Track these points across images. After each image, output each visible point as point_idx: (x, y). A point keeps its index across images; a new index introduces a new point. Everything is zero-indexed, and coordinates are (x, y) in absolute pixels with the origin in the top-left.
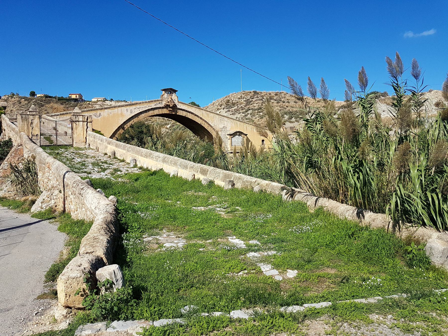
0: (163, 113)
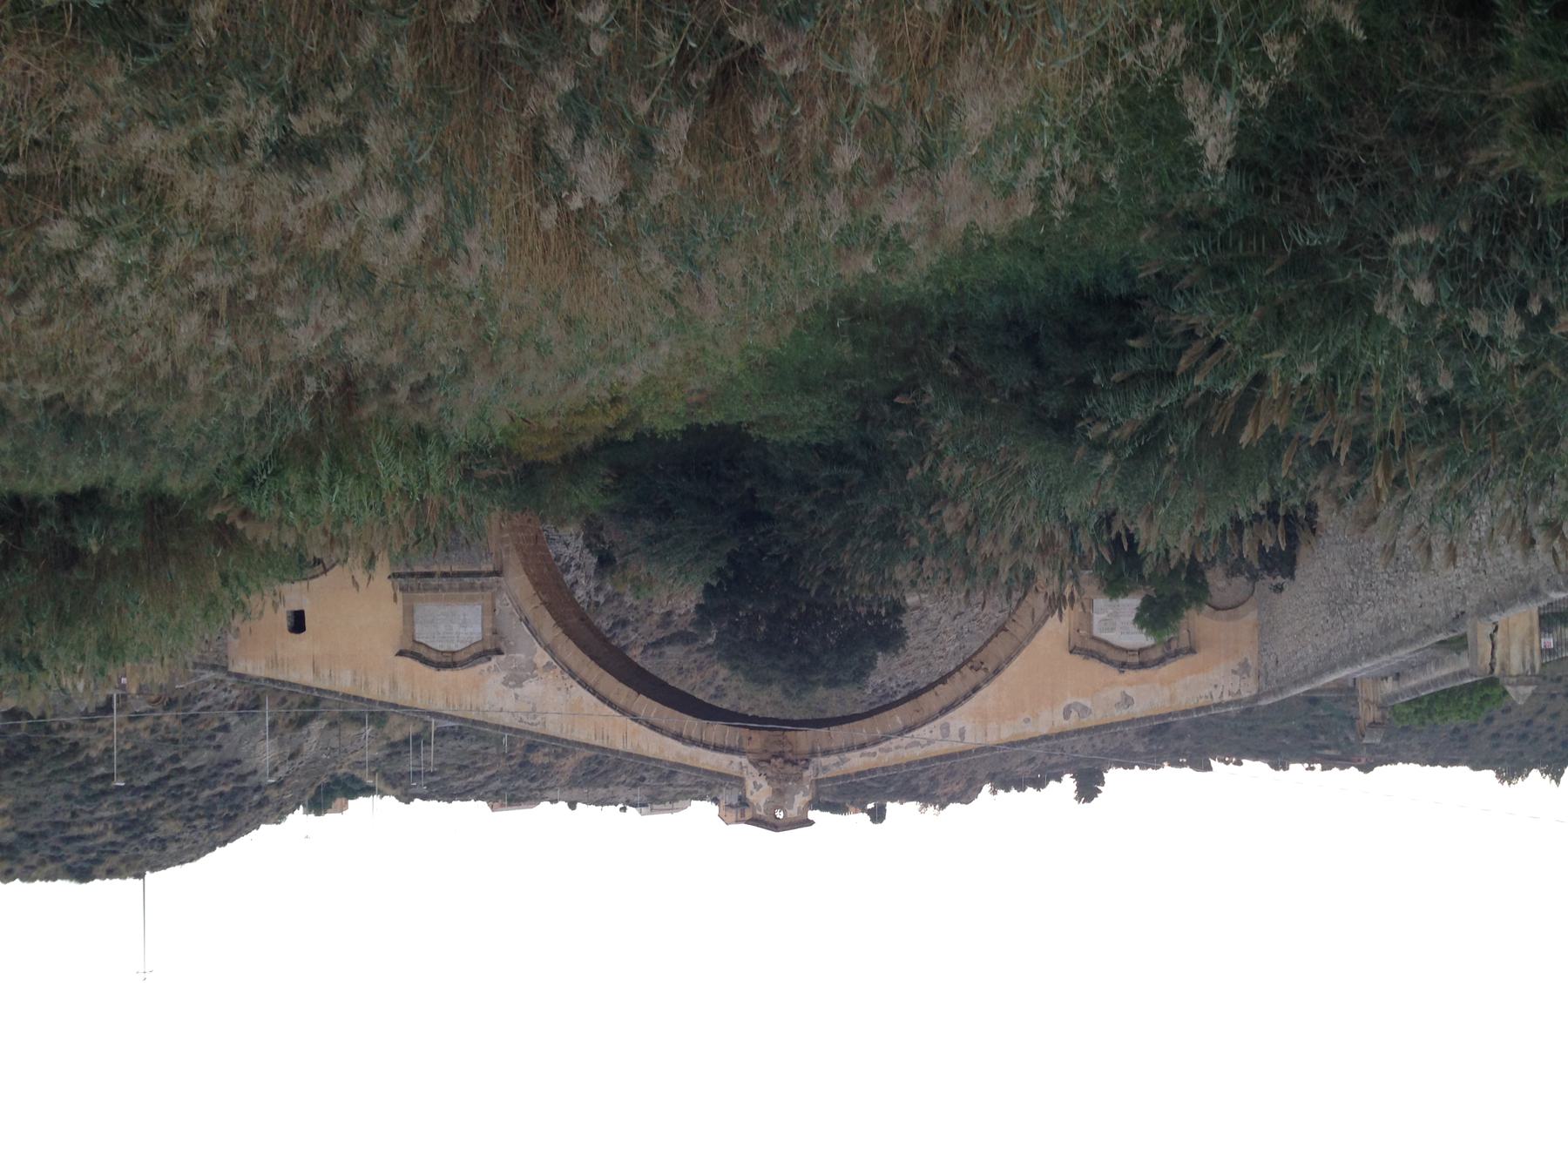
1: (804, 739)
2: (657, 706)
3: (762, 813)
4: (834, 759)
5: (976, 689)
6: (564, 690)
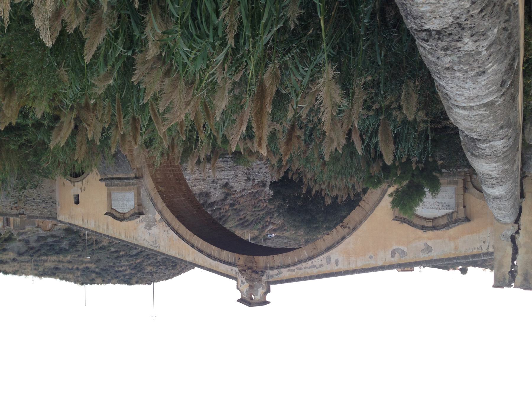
0: (265, 257)
1: (262, 260)
2: (201, 241)
3: (245, 296)
4: (275, 271)
5: (343, 238)
6: (166, 231)
